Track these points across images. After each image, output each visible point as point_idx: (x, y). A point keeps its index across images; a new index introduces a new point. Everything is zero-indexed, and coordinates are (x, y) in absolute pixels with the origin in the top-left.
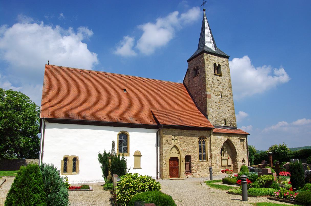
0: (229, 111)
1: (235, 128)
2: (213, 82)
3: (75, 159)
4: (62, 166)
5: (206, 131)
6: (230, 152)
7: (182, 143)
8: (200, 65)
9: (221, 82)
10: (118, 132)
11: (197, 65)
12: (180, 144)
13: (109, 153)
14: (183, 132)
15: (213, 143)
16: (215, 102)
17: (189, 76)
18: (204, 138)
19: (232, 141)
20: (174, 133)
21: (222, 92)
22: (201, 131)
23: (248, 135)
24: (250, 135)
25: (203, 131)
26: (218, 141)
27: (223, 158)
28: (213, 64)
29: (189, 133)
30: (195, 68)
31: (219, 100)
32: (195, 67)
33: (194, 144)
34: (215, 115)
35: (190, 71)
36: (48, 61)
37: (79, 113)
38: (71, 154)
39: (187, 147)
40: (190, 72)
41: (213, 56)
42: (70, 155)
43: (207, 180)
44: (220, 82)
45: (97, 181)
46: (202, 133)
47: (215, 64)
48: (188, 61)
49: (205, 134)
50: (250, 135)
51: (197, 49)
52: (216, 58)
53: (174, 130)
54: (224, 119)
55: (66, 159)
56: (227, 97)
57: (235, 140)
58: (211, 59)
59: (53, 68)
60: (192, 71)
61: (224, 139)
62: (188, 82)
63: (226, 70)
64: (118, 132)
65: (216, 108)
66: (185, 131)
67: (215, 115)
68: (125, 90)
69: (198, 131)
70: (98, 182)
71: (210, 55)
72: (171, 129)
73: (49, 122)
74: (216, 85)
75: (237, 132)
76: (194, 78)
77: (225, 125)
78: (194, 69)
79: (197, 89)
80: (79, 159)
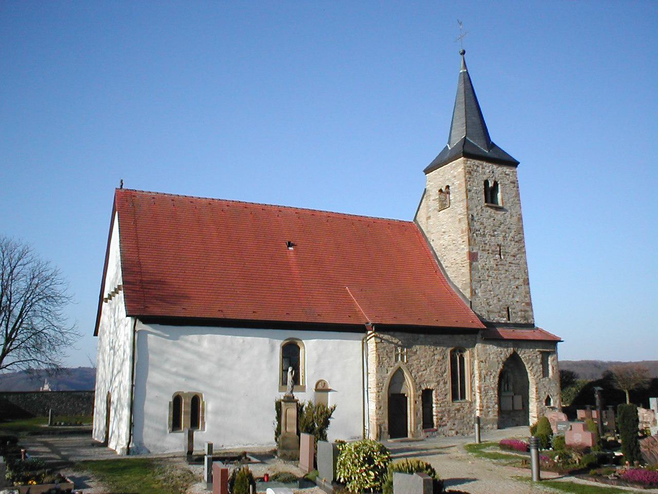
1: (531, 326)
2: (482, 224)
3: (196, 400)
8: (453, 184)
10: (282, 341)
13: (577, 377)
14: (418, 339)
18: (462, 350)
22: (456, 336)
23: (559, 343)
24: (563, 341)
25: (461, 336)
28: (483, 182)
32: (442, 187)
38: (188, 388)
42: (186, 391)
43: (460, 297)
45: (240, 444)
46: (459, 340)
47: (486, 183)
49: (464, 342)
50: (563, 341)
52: (489, 167)
54: (506, 307)
55: (177, 401)
56: (514, 256)
62: (425, 219)
64: (282, 341)
65: (490, 282)
66: (422, 336)
68: (290, 245)
69: (451, 336)
70: (242, 446)
71: (477, 162)
75: (538, 336)
77: (509, 320)
79: (446, 237)
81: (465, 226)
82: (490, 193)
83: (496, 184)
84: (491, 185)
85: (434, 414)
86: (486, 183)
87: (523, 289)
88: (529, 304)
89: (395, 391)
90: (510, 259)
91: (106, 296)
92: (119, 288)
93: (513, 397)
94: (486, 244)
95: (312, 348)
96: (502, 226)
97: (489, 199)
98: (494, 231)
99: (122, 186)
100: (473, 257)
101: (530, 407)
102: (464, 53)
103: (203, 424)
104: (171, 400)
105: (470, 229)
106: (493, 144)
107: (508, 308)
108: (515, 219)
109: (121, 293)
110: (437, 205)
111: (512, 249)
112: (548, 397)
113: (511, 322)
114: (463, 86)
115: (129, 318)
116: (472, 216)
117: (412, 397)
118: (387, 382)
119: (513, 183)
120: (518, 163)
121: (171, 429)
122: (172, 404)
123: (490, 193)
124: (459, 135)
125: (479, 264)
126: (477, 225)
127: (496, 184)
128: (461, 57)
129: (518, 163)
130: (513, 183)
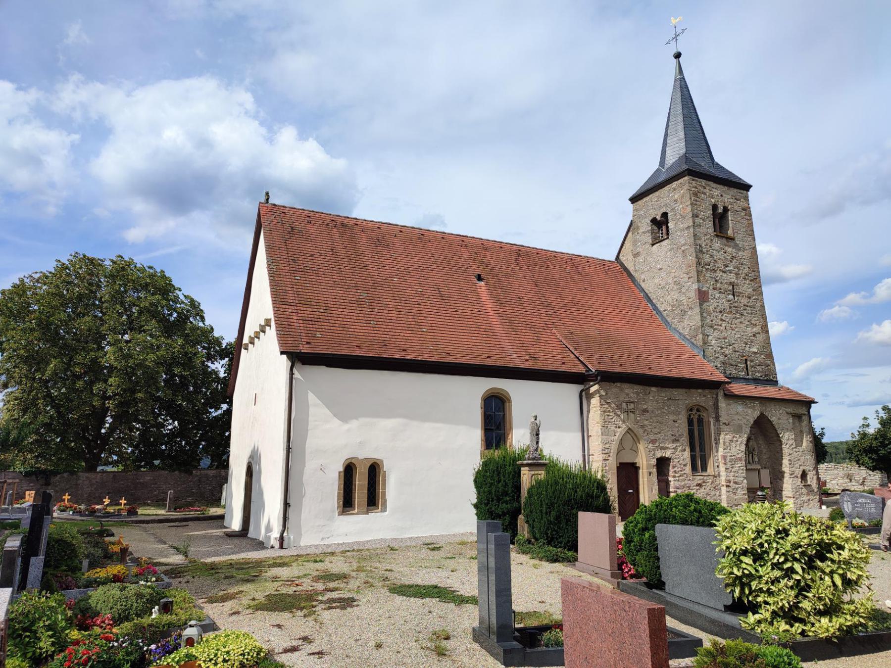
0: (754, 335)
2: (712, 256)
3: (374, 470)
4: (339, 489)
5: (707, 391)
6: (765, 450)
7: (646, 423)
9: (733, 258)
11: (664, 210)
12: (642, 427)
15: (725, 423)
16: (720, 312)
17: (635, 242)
19: (773, 419)
20: (627, 395)
21: (737, 285)
25: (699, 391)
26: (736, 417)
27: (236, 524)
28: (711, 207)
29: (663, 395)
30: (658, 218)
31: (730, 307)
33: (677, 425)
34: (722, 348)
35: (638, 228)
36: (267, 194)
37: (360, 340)
39: (659, 435)
40: (641, 231)
41: (710, 183)
42: (361, 456)
44: (729, 258)
47: (715, 207)
48: (634, 199)
51: (656, 165)
53: (625, 385)
55: (349, 470)
56: (749, 298)
57: (778, 417)
58: (705, 194)
59: (280, 212)
60: (645, 225)
61: (752, 414)
63: (746, 223)
65: (723, 328)
66: (654, 389)
67: (722, 348)
71: (703, 182)
72: (619, 384)
73: (303, 364)
74: (720, 264)
76: (655, 246)
78: (654, 221)
80: (386, 466)
81: (692, 259)
82: (720, 218)
83: (726, 210)
84: (720, 210)
85: (671, 490)
86: (715, 207)
87: (760, 337)
88: (770, 356)
89: (628, 459)
90: (744, 301)
91: (246, 340)
92: (268, 323)
93: (759, 471)
94: (716, 281)
95: (525, 398)
96: (734, 261)
97: (718, 230)
98: (726, 266)
99: (267, 199)
100: (703, 296)
101: (785, 486)
102: (678, 56)
103: (385, 502)
104: (342, 469)
105: (699, 263)
106: (718, 164)
107: (746, 360)
108: (747, 254)
109: (272, 333)
110: (648, 238)
111: (746, 288)
112: (804, 471)
113: (750, 377)
114: (679, 95)
115: (285, 357)
116: (700, 246)
117: (645, 467)
118: (614, 447)
119: (744, 209)
120: (750, 186)
121: (341, 509)
122: (342, 474)
123: (720, 218)
124: (677, 150)
125: (711, 305)
126: (707, 258)
127: (726, 210)
128: (675, 60)
129: (750, 186)
130: (744, 209)
